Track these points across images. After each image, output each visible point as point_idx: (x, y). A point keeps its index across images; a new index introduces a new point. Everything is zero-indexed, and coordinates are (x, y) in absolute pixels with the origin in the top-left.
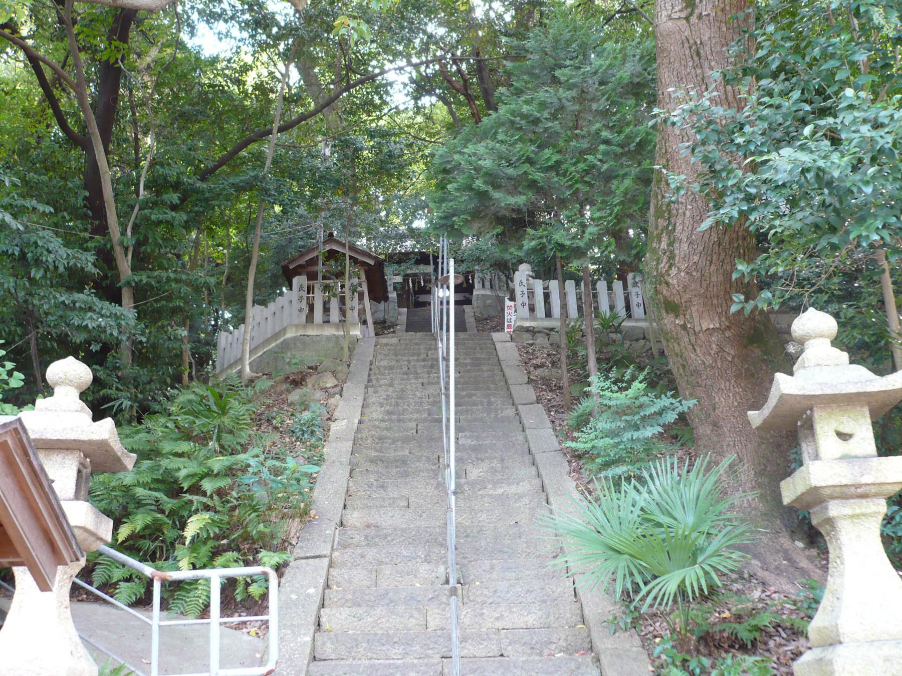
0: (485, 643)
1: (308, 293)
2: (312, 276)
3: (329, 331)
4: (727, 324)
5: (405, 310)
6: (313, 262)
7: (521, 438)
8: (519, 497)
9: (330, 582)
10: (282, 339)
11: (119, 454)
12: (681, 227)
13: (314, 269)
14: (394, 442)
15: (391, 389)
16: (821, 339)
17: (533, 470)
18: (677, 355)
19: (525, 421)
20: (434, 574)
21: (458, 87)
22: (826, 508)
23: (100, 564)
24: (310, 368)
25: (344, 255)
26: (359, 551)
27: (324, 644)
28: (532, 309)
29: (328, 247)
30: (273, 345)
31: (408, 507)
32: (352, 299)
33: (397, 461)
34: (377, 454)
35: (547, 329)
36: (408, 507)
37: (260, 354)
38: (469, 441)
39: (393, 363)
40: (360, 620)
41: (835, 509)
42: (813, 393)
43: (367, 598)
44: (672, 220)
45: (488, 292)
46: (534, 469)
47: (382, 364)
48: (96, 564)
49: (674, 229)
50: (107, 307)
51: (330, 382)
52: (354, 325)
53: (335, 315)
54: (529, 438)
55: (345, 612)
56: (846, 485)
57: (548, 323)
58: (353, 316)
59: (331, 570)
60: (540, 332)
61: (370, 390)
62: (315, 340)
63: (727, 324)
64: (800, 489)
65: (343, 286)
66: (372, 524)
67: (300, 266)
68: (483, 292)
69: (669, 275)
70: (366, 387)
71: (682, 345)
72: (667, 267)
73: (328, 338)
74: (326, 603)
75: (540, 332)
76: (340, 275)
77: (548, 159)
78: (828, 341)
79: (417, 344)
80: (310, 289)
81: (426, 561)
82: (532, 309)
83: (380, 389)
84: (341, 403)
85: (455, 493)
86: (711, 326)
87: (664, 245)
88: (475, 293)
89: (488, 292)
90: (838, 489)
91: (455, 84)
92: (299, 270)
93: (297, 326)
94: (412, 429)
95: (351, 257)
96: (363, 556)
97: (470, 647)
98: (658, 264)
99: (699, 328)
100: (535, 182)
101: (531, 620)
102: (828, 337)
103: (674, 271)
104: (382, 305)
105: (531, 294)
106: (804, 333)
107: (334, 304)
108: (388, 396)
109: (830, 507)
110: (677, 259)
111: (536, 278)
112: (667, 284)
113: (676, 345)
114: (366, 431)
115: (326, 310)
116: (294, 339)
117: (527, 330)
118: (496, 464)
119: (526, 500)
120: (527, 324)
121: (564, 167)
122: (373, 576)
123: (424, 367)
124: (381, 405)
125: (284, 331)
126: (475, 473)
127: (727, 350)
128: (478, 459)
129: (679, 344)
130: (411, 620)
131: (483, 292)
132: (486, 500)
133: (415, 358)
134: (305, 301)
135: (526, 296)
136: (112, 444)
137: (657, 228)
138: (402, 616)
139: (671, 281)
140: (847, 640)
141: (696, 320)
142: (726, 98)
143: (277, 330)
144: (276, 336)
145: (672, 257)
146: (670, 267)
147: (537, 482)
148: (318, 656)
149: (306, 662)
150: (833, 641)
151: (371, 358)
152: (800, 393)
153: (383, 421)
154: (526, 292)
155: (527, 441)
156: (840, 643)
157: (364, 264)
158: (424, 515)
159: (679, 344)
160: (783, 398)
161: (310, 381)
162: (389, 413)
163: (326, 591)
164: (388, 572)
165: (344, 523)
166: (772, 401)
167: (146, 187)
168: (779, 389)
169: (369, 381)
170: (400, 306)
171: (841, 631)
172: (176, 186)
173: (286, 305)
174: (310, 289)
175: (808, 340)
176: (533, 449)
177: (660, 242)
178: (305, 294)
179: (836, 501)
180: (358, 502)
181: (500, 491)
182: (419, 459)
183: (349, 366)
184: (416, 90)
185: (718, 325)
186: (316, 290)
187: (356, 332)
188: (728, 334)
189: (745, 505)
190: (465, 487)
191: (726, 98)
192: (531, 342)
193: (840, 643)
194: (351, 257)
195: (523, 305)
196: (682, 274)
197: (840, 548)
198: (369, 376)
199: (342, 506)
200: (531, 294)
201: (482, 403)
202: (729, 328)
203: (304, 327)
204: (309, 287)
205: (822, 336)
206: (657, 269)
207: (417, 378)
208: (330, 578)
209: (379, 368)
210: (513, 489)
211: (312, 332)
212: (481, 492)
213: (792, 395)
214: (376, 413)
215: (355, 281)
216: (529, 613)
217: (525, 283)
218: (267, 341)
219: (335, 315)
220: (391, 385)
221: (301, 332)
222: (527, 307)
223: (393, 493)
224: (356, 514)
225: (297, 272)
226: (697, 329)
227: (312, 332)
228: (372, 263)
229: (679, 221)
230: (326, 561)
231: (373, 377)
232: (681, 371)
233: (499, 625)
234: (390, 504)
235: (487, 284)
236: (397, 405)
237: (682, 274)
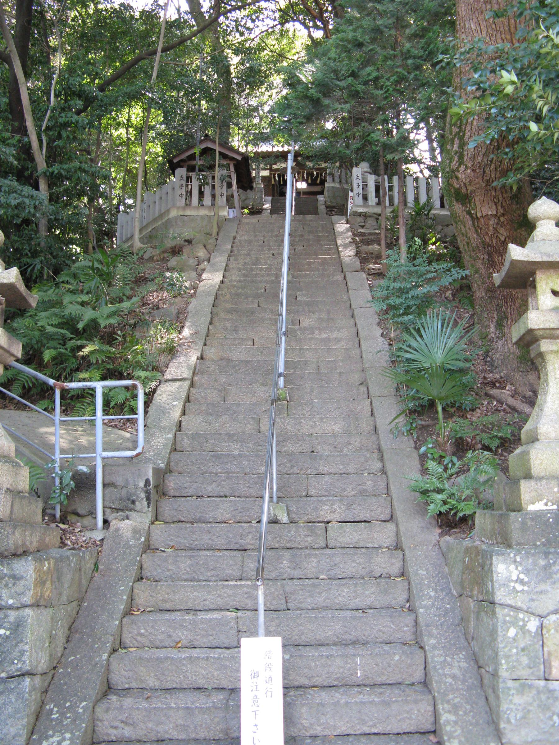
0: (301, 443)
1: (187, 182)
2: (191, 169)
3: (203, 212)
4: (502, 211)
5: (270, 198)
6: (192, 157)
7: (345, 297)
8: (337, 340)
9: (190, 398)
10: (166, 219)
11: (24, 294)
12: (469, 134)
13: (194, 163)
14: (247, 297)
15: (248, 258)
16: (548, 221)
17: (352, 322)
18: (463, 234)
19: (349, 284)
20: (268, 394)
21: (315, 14)
22: (539, 345)
23: (19, 380)
24: (186, 241)
25: (215, 150)
26: (214, 377)
27: (182, 440)
28: (365, 198)
29: (203, 146)
30: (160, 223)
31: (253, 345)
32: (222, 186)
33: (248, 312)
34: (233, 306)
35: (376, 214)
36: (253, 345)
37: (150, 230)
38: (305, 299)
39: (253, 238)
40: (210, 424)
41: (545, 346)
42: (533, 260)
43: (216, 409)
44: (463, 127)
45: (338, 185)
46: (352, 320)
47: (243, 238)
48: (16, 379)
49: (464, 134)
50: (27, 190)
51: (202, 253)
52: (222, 207)
53: (207, 200)
54: (351, 297)
55: (200, 418)
56: (553, 329)
57: (378, 210)
58: (222, 201)
59: (191, 389)
60: (370, 216)
61: (232, 259)
62: (193, 219)
63: (502, 211)
64: (522, 331)
65: (213, 177)
66: (225, 358)
67: (182, 161)
68: (332, 185)
69: (459, 171)
70: (229, 256)
71: (467, 226)
72: (457, 164)
73: (202, 217)
74: (187, 412)
75: (370, 216)
76: (211, 167)
77: (369, 74)
78: (553, 222)
79: (271, 223)
80: (189, 179)
81: (263, 385)
82: (365, 198)
83: (239, 258)
84: (208, 268)
85: (285, 334)
86: (490, 213)
87: (456, 147)
88: (326, 185)
89: (338, 185)
90: (548, 331)
91: (313, 12)
92: (182, 164)
93: (178, 208)
94: (261, 289)
95: (220, 153)
96: (216, 380)
97: (289, 445)
98: (450, 162)
99: (480, 214)
100: (357, 92)
101: (337, 428)
102: (554, 219)
103: (462, 168)
104: (250, 193)
105: (365, 186)
106: (536, 215)
107: (207, 190)
108: (245, 263)
109: (542, 344)
110: (465, 158)
111: (371, 174)
112: (457, 178)
113: (462, 227)
114: (226, 290)
115: (201, 194)
116: (176, 218)
117: (360, 214)
118: (324, 315)
119: (343, 343)
120: (361, 210)
121: (382, 81)
122: (223, 395)
123: (276, 241)
124: (239, 270)
125: (168, 211)
126: (306, 322)
127: (501, 232)
128: (310, 312)
129: (465, 226)
130: (248, 426)
131: (332, 185)
132: (312, 342)
133: (270, 234)
134: (184, 188)
135: (361, 187)
136: (18, 286)
137: (451, 134)
138: (241, 423)
139: (460, 176)
140: (543, 438)
141: (478, 207)
142: (509, 30)
143: (163, 211)
144: (161, 216)
145: (461, 157)
146: (460, 165)
147: (354, 330)
148: (178, 448)
149: (168, 451)
150: (534, 439)
151: (235, 234)
152: (525, 259)
153: (240, 281)
154: (361, 184)
155: (349, 299)
156: (538, 440)
157: (232, 159)
158: (265, 352)
159: (465, 226)
160: (514, 263)
161: (186, 251)
162: (244, 275)
163: (187, 404)
164: (234, 392)
165: (204, 356)
166: (507, 265)
167: (56, 96)
168: (510, 256)
169: (231, 252)
170: (266, 195)
171: (539, 432)
172: (80, 95)
173: (170, 191)
174: (189, 179)
175: (539, 221)
176: (353, 306)
177: (453, 144)
178: (184, 183)
179: (546, 341)
180: (215, 341)
181: (325, 336)
182: (265, 310)
183: (217, 239)
184: (281, 17)
185: (495, 212)
186: (193, 180)
187: (225, 213)
188: (502, 219)
189: (506, 350)
190: (298, 332)
191: (509, 30)
192: (363, 224)
193: (538, 440)
194: (220, 153)
195: (358, 194)
196: (469, 171)
197: (547, 375)
198: (232, 247)
199: (203, 343)
200: (365, 186)
201: (318, 270)
202: (503, 215)
203: (184, 209)
204: (188, 178)
205: (549, 218)
206: (450, 165)
207: (269, 250)
208: (191, 395)
209: (240, 241)
210: (335, 335)
211: (188, 212)
212: (309, 336)
213: (519, 261)
214: (235, 276)
215: (225, 172)
216: (335, 423)
217: (360, 177)
218: (155, 220)
219: (207, 200)
220: (249, 255)
221: (181, 213)
222: (361, 197)
223: (242, 335)
224: (213, 350)
225: (179, 165)
226: (479, 215)
227: (188, 212)
228: (239, 158)
229: (468, 128)
230: (187, 384)
231: (235, 249)
232: (466, 247)
233: (312, 431)
234: (239, 343)
235: (337, 179)
236: (252, 270)
237: (469, 171)
